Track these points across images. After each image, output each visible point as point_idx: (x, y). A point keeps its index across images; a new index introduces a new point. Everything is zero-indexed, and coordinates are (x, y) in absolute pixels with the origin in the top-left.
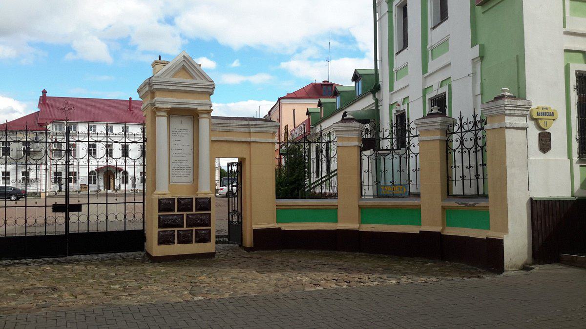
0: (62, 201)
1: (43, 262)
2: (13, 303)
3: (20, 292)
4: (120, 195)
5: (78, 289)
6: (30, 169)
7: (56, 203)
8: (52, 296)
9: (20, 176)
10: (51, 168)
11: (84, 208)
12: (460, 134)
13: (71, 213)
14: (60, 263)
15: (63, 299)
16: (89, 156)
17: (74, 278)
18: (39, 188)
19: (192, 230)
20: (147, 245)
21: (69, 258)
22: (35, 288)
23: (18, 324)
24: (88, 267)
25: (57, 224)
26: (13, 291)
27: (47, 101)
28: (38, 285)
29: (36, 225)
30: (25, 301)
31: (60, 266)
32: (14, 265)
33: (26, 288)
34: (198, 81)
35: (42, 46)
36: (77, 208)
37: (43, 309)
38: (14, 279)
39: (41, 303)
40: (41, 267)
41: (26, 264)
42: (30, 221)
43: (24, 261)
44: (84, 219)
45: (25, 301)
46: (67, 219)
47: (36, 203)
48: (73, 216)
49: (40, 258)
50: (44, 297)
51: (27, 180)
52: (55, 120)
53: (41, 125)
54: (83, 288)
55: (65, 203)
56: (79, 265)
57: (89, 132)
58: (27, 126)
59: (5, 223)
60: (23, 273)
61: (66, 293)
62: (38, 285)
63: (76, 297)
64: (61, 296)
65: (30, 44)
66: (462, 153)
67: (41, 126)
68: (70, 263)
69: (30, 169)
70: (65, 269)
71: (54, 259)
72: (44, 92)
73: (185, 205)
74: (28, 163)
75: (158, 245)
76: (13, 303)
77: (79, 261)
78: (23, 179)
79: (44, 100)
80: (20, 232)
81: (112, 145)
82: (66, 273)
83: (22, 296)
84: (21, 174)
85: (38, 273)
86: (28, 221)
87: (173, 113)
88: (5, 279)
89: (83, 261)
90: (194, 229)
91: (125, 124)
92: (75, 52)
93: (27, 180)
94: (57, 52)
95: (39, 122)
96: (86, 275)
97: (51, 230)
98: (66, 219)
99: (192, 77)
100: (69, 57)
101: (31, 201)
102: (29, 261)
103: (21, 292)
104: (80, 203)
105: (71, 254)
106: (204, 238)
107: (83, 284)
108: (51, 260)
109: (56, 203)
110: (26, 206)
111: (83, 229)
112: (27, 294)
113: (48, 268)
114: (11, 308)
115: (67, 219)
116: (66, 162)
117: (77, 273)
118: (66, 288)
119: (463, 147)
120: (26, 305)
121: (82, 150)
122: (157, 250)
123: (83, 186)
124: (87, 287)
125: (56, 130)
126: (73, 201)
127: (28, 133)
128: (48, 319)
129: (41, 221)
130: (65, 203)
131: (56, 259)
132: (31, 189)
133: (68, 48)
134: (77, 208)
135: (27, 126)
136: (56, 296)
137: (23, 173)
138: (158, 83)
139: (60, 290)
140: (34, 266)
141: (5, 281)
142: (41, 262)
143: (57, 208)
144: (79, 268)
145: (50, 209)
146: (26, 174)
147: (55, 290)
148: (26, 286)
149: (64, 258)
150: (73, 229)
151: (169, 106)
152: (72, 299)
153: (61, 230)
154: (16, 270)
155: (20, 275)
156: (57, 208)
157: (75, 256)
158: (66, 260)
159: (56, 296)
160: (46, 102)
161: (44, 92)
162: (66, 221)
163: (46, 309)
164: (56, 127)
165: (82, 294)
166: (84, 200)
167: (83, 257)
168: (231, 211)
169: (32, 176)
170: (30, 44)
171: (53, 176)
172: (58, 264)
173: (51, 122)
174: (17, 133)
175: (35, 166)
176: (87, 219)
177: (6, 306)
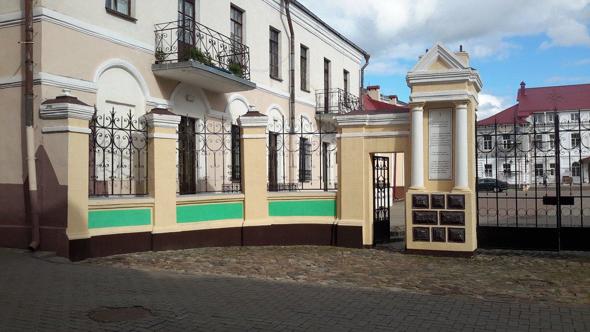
0: (553, 194)
1: (535, 254)
2: (511, 292)
3: (516, 282)
4: (576, 189)
5: (575, 286)
6: (511, 162)
7: (546, 195)
8: (549, 290)
9: (502, 169)
10: (531, 160)
11: (577, 201)
12: (203, 132)
13: (562, 206)
14: (552, 257)
15: (561, 295)
16: (535, 150)
17: (570, 275)
18: (521, 180)
19: (445, 228)
20: (404, 240)
21: (561, 252)
22: (531, 280)
23: (433, 306)
24: (584, 264)
25: (548, 216)
26: (510, 279)
27: (526, 94)
28: (533, 276)
29: (526, 217)
30: (522, 291)
31: (553, 260)
32: (506, 254)
33: (522, 278)
34: (454, 70)
35: (517, 39)
36: (569, 201)
37: (541, 302)
38: (509, 268)
39: (539, 295)
40: (533, 259)
41: (518, 255)
42: (521, 213)
43: (515, 251)
44: (577, 213)
45: (522, 291)
46: (559, 212)
47: (526, 195)
48: (565, 209)
49: (532, 250)
50: (541, 290)
51: (507, 172)
52: (535, 111)
53: (520, 118)
54: (582, 286)
55: (556, 196)
56: (574, 261)
57: (534, 123)
58: (496, 119)
59: (497, 213)
60: (516, 263)
61: (564, 289)
62: (533, 277)
63: (575, 295)
64: (558, 291)
65: (505, 40)
66: (113, 152)
67: (520, 118)
68: (563, 258)
69: (511, 162)
70: (559, 264)
71: (545, 252)
72: (523, 84)
73: (437, 201)
74: (537, 155)
75: (414, 241)
76: (511, 292)
77: (573, 257)
78: (505, 171)
79: (523, 92)
80: (512, 223)
81: (541, 136)
82: (560, 268)
83: (519, 285)
84: (502, 167)
85: (531, 264)
86: (584, 212)
87: (429, 108)
88: (500, 267)
89: (577, 257)
90: (447, 227)
91: (579, 111)
92: (550, 40)
93: (507, 172)
94: (532, 43)
95: (519, 114)
96: (583, 272)
97: (542, 223)
98: (557, 212)
99: (448, 67)
100: (544, 46)
101: (511, 192)
102: (520, 252)
103: (517, 282)
104: (572, 195)
105: (563, 248)
106: (458, 237)
107: (581, 282)
108: (542, 252)
109: (546, 195)
110: (516, 198)
111: (577, 223)
112: (523, 285)
113: (541, 261)
114: (509, 295)
115: (559, 212)
116: (556, 153)
117: (573, 269)
118: (563, 284)
119: (114, 147)
120: (524, 295)
121: (566, 139)
122: (411, 244)
123: (566, 179)
124: (585, 285)
125: (551, 120)
126: (564, 194)
127: (497, 127)
128: (551, 313)
129: (532, 212)
130: (556, 196)
131: (547, 252)
132: (512, 181)
133: (544, 37)
134: (569, 201)
135: (496, 119)
136: (553, 290)
137: (505, 166)
138: (415, 77)
139: (556, 285)
140: (526, 257)
141: (501, 269)
142: (532, 254)
143: (547, 200)
144: (574, 264)
145: (540, 201)
146: (507, 166)
147: (551, 284)
148: (522, 276)
149: (556, 253)
150: (565, 223)
151: (424, 100)
152: (570, 296)
153: (553, 223)
154: (509, 260)
155: (513, 265)
156: (547, 200)
157: (567, 252)
158: (558, 255)
159: (553, 290)
160: (524, 93)
161: (523, 84)
162: (557, 214)
163: (545, 302)
164: (551, 117)
165: (581, 292)
166: (576, 193)
167: (576, 253)
168: (376, 208)
169: (513, 168)
170: (505, 40)
171: (534, 169)
172: (550, 258)
173: (530, 114)
174: (525, 126)
175: (514, 159)
176: (580, 212)
177: (505, 293)
